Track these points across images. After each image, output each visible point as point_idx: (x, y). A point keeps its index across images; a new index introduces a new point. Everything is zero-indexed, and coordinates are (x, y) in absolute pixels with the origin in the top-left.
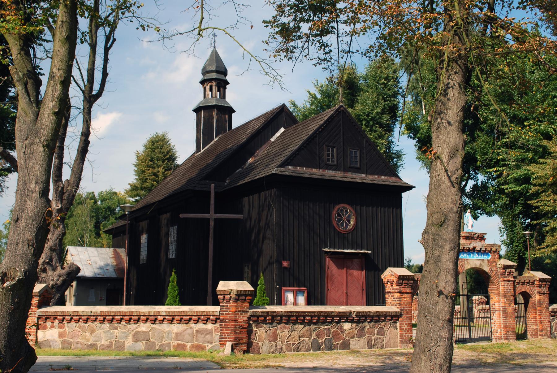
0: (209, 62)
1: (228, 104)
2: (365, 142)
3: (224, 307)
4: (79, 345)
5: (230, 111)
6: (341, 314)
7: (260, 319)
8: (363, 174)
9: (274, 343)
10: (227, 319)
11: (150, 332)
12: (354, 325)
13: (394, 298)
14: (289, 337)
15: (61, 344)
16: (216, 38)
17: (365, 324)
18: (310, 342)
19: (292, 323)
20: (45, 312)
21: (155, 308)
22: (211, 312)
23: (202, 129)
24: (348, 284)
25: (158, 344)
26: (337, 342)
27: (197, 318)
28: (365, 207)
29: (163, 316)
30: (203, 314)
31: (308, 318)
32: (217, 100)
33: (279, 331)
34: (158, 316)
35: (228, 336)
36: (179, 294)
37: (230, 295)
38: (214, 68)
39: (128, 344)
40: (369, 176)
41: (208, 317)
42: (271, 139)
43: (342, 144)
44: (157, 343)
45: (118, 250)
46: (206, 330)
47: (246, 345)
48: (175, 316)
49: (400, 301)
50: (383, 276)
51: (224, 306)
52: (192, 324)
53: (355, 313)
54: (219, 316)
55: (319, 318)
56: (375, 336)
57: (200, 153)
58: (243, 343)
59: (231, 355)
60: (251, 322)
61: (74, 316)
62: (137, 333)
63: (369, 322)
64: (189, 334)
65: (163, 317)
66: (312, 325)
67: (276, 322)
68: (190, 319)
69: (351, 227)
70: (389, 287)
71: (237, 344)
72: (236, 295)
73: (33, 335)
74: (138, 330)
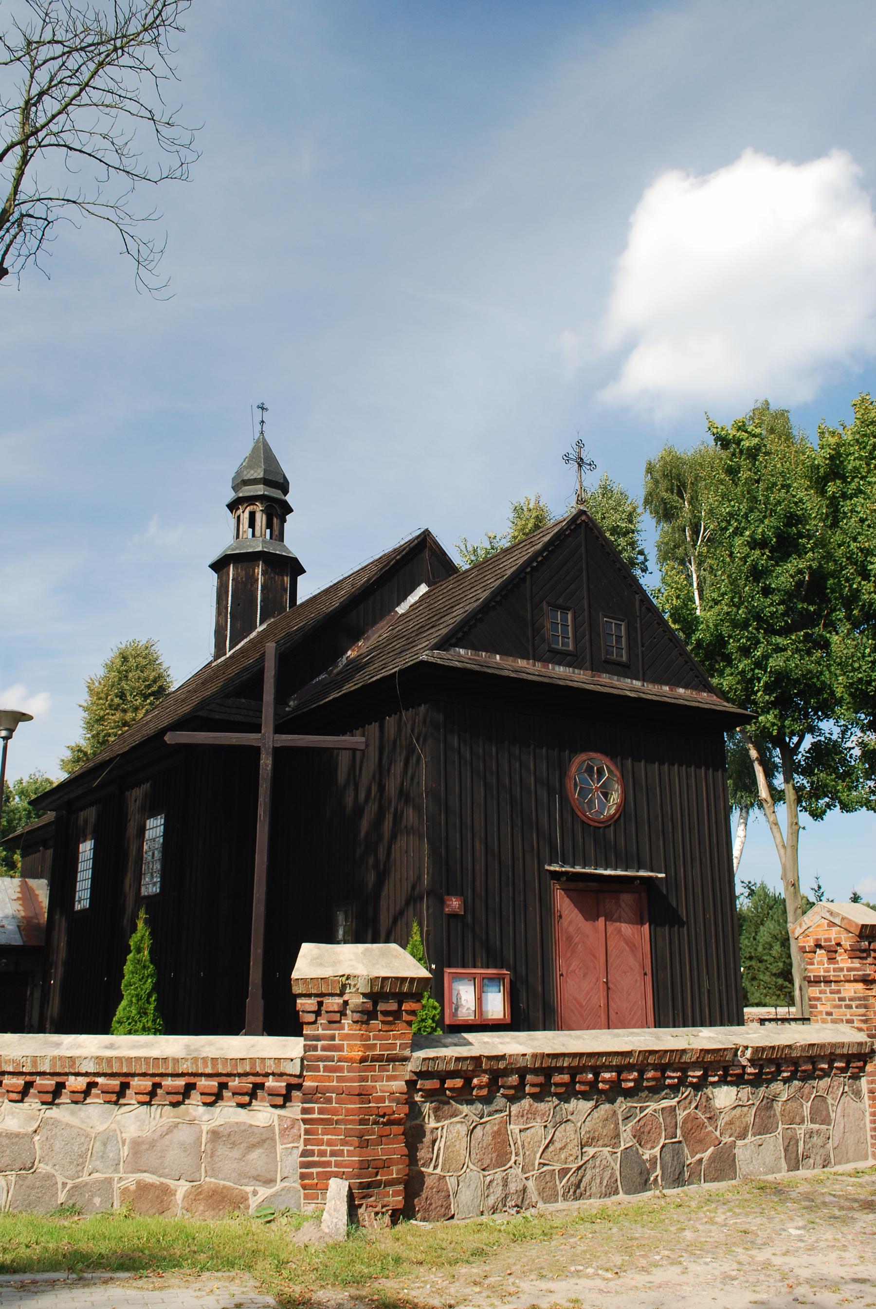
0: (249, 461)
1: (290, 552)
2: (637, 603)
3: (320, 1044)
5: (294, 568)
6: (709, 1058)
7: (449, 1083)
8: (637, 679)
9: (498, 1174)
10: (332, 1090)
11: (37, 1138)
13: (840, 999)
14: (547, 1147)
16: (267, 416)
17: (777, 1087)
18: (615, 1160)
19: (556, 1095)
21: (58, 1045)
22: (268, 1062)
23: (229, 605)
24: (610, 961)
25: (64, 1184)
26: (698, 1156)
27: (214, 1083)
28: (643, 763)
29: (87, 1074)
30: (240, 1071)
31: (607, 1075)
32: (264, 542)
33: (514, 1128)
34: (67, 1074)
35: (333, 1154)
36: (156, 988)
37: (341, 994)
38: (260, 474)
40: (650, 686)
41: (258, 1080)
42: (397, 609)
43: (586, 602)
44: (60, 1180)
45: (32, 882)
47: (401, 1187)
48: (133, 1075)
49: (866, 1007)
51: (317, 1038)
52: (195, 1108)
53: (748, 1054)
54: (301, 1076)
55: (641, 1073)
56: (804, 1127)
57: (223, 658)
58: (390, 1183)
59: (348, 1234)
60: (418, 1098)
63: (786, 1081)
65: (86, 1080)
66: (620, 1099)
67: (504, 1096)
68: (190, 1087)
69: (612, 811)
70: (821, 963)
71: (369, 1185)
72: (365, 995)
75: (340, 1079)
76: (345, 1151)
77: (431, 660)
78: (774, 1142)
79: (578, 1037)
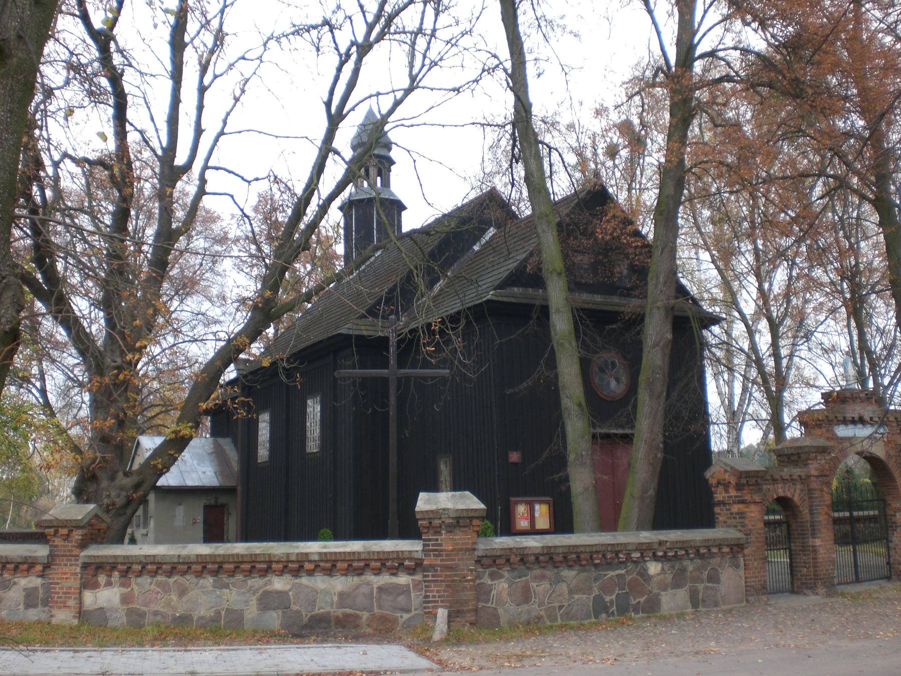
1: (395, 196)
4: (159, 618)
12: (667, 566)
15: (127, 615)
20: (94, 556)
21: (297, 547)
39: (250, 616)
45: (221, 441)
46: (397, 586)
50: (708, 474)
51: (429, 540)
52: (370, 577)
61: (147, 564)
62: (266, 593)
64: (364, 594)
73: (75, 599)
74: (268, 588)
75: (441, 560)
76: (392, 361)
77: (494, 298)
78: (682, 594)
79: (569, 537)
